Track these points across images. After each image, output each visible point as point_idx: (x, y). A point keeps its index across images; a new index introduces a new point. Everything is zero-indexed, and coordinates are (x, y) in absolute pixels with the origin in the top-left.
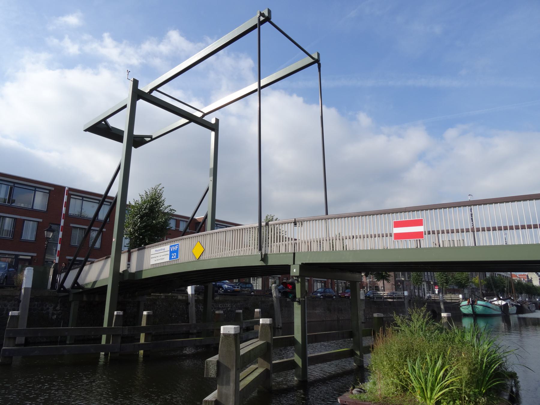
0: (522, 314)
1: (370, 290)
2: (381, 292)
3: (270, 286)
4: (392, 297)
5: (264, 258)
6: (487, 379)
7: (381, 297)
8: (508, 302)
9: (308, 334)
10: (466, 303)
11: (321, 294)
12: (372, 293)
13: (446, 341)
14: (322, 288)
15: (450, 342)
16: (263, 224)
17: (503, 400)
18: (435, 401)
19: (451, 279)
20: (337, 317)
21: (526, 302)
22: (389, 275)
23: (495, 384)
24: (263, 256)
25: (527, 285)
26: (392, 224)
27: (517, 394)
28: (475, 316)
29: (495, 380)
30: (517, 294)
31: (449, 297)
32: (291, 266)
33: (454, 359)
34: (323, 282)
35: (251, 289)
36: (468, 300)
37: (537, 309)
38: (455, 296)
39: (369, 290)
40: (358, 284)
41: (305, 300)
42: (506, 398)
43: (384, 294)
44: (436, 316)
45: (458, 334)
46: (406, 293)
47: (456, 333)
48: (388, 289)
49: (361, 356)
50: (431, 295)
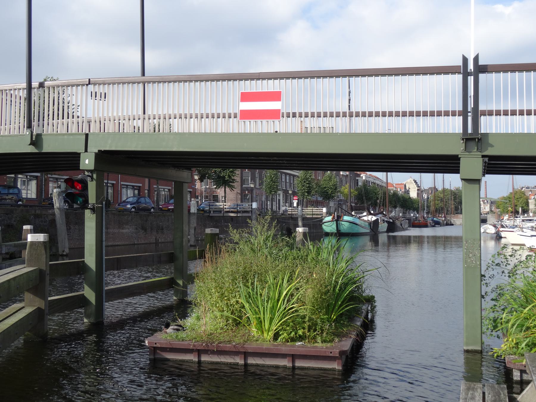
0: (393, 232)
1: (205, 201)
2: (221, 204)
3: (50, 192)
4: (236, 210)
5: (36, 141)
6: (340, 303)
7: (220, 211)
8: (379, 218)
9: (106, 258)
10: (330, 218)
11: (132, 206)
12: (208, 204)
13: (297, 260)
14: (134, 196)
15: (302, 261)
16: (35, 84)
17: (355, 326)
18: (274, 333)
19: (315, 187)
20: (156, 239)
21: (399, 218)
22: (233, 180)
23: (348, 308)
24: (34, 137)
25: (403, 197)
26: (238, 96)
27: (372, 321)
28: (340, 235)
29: (348, 304)
30: (391, 208)
31: (309, 211)
32: (81, 154)
33: (303, 281)
34: (135, 187)
35: (17, 196)
36: (333, 215)
37: (410, 226)
38: (317, 210)
39: (205, 201)
40: (187, 189)
41: (102, 207)
42: (359, 324)
43: (225, 207)
44: (290, 232)
45: (312, 251)
46: (255, 205)
47: (311, 250)
48: (231, 200)
49: (185, 286)
50: (288, 208)
